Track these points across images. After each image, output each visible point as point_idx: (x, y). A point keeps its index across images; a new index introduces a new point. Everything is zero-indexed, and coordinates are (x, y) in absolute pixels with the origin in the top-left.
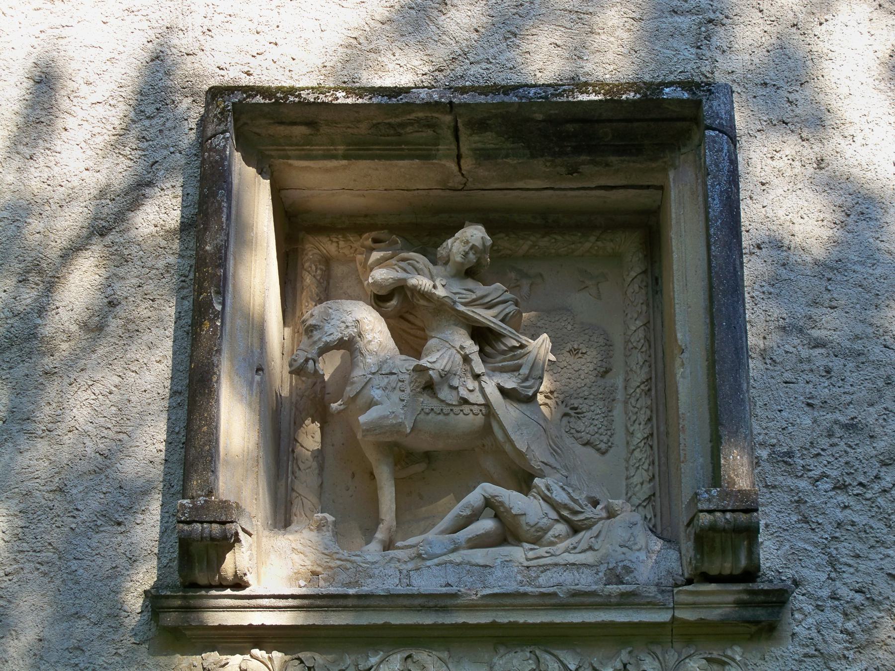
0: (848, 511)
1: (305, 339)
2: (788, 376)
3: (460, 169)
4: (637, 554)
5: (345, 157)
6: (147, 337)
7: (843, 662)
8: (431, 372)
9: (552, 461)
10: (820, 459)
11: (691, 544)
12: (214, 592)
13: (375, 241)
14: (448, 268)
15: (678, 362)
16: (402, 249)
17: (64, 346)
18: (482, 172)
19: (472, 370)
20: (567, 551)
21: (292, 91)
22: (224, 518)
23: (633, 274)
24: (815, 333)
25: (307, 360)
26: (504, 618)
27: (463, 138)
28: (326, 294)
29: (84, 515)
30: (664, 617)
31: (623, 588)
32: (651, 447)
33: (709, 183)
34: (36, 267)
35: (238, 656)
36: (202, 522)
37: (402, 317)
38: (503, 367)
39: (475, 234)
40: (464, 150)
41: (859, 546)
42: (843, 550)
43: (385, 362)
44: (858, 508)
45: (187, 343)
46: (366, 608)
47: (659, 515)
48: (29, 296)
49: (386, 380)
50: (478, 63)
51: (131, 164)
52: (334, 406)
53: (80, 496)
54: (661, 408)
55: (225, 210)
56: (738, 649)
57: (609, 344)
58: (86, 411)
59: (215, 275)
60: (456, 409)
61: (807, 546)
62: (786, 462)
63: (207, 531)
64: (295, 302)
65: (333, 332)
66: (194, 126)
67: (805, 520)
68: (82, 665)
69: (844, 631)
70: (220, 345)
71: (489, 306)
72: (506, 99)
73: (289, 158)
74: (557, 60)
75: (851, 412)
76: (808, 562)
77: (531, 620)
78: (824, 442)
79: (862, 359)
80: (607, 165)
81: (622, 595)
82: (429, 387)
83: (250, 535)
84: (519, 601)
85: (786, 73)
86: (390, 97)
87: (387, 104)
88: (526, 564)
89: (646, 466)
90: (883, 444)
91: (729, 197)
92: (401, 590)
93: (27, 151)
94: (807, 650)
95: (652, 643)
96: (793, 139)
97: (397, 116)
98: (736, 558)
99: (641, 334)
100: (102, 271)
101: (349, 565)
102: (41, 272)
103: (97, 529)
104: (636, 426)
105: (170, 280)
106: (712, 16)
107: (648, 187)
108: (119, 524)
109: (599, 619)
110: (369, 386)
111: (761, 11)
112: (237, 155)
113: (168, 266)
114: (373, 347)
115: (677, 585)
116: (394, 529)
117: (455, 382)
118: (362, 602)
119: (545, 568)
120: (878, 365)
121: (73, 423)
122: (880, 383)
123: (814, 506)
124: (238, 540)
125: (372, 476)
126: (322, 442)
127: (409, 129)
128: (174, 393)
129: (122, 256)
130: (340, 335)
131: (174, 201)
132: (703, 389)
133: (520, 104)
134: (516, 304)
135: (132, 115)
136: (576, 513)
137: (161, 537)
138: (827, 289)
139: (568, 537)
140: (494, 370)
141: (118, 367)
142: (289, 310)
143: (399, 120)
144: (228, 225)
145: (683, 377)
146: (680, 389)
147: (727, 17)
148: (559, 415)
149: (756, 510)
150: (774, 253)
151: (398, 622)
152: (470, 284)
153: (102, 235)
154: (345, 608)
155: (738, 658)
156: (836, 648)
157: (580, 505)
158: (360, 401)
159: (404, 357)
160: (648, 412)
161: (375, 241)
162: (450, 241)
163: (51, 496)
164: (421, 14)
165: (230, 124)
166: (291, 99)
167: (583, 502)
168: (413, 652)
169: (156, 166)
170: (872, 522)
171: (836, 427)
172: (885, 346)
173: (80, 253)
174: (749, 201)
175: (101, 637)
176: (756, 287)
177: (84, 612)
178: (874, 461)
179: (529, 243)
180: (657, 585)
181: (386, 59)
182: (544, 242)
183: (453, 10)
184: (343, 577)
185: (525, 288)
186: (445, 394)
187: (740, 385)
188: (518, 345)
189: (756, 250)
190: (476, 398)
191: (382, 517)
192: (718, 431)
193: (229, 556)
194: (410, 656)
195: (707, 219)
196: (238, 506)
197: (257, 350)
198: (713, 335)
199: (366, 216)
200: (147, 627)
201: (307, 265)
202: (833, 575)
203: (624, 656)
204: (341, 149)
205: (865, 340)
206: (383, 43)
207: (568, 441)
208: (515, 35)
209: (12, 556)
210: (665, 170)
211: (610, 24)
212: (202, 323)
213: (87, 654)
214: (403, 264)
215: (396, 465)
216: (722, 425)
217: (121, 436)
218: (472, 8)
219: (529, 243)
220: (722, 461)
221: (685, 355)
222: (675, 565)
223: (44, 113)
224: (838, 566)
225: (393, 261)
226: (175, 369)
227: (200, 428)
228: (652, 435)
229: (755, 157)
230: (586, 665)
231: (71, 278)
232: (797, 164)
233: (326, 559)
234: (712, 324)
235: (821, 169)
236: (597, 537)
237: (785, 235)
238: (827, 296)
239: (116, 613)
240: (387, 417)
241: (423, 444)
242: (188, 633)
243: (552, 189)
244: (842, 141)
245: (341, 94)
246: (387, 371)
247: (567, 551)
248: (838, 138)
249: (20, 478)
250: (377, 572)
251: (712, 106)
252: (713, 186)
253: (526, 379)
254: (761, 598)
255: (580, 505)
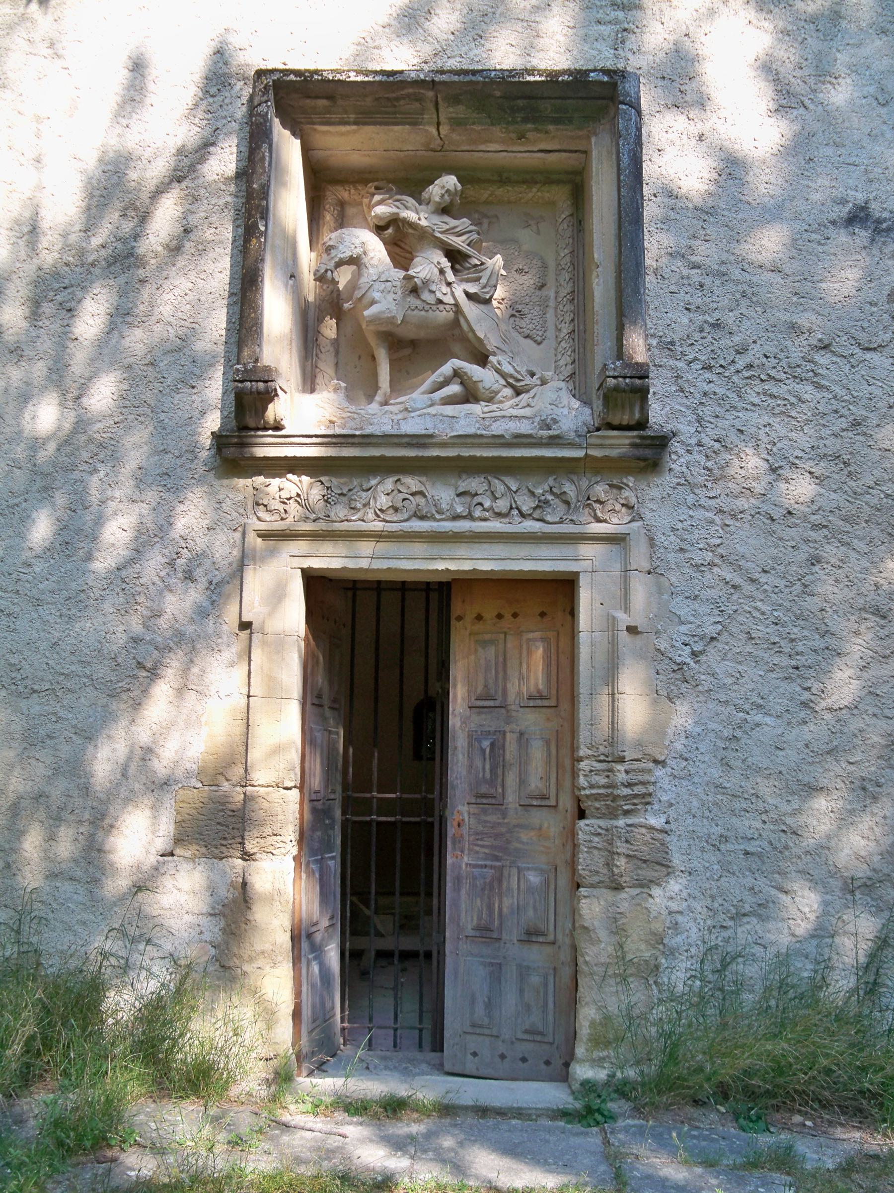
0: (711, 385)
1: (325, 256)
2: (673, 288)
3: (439, 134)
4: (562, 410)
5: (355, 123)
6: (212, 255)
7: (704, 489)
8: (416, 280)
9: (502, 346)
10: (694, 347)
11: (600, 402)
12: (260, 433)
13: (377, 188)
14: (429, 206)
15: (595, 274)
16: (396, 194)
17: (153, 261)
18: (455, 136)
19: (446, 279)
20: (512, 407)
21: (316, 72)
22: (266, 378)
23: (563, 216)
24: (694, 259)
25: (326, 271)
26: (466, 453)
27: (441, 110)
28: (342, 223)
29: (169, 381)
30: (580, 453)
31: (551, 432)
32: (573, 339)
33: (621, 143)
34: (132, 206)
35: (277, 479)
36: (251, 381)
37: (396, 244)
38: (468, 278)
39: (450, 181)
40: (442, 119)
41: (718, 409)
42: (707, 412)
43: (383, 273)
44: (719, 382)
45: (240, 259)
46: (368, 445)
47: (577, 388)
48: (128, 227)
49: (383, 286)
50: (454, 57)
51: (199, 130)
52: (346, 306)
53: (165, 368)
54: (581, 313)
55: (267, 158)
56: (631, 479)
57: (545, 266)
58: (168, 308)
59: (260, 205)
60: (434, 307)
61: (682, 408)
62: (669, 349)
63: (255, 387)
64: (318, 230)
65: (345, 252)
66: (245, 102)
67: (682, 390)
68: (169, 486)
69: (706, 468)
70: (264, 255)
71: (459, 235)
72: (474, 78)
73: (314, 124)
74: (512, 56)
75: (717, 315)
76: (682, 420)
77: (485, 455)
78: (697, 336)
79: (726, 278)
80: (547, 132)
81: (551, 437)
82: (415, 291)
83: (286, 392)
84: (477, 441)
85: (679, 71)
86: (388, 76)
87: (386, 82)
88: (482, 416)
89: (569, 353)
90: (738, 338)
91: (635, 154)
92: (394, 432)
93: (124, 122)
94: (679, 480)
95: (570, 473)
96: (682, 119)
97: (393, 92)
98: (632, 413)
99: (568, 259)
100: (179, 208)
101: (356, 416)
102: (136, 209)
103: (177, 391)
104: (563, 325)
105: (229, 215)
106: (626, 26)
107: (576, 151)
108: (193, 387)
109: (533, 455)
110: (371, 290)
111: (662, 23)
112: (276, 121)
113: (226, 203)
114: (375, 262)
115: (589, 432)
116: (388, 394)
117: (433, 288)
118: (364, 440)
119: (495, 419)
120: (737, 282)
121: (159, 316)
122: (738, 296)
123: (688, 380)
124: (277, 395)
125: (373, 358)
126: (337, 334)
127: (402, 102)
128: (231, 295)
129: (194, 197)
130: (350, 254)
131: (231, 157)
132: (612, 294)
133: (484, 83)
134: (478, 234)
135: (200, 94)
136: (518, 380)
137: (223, 396)
138: (702, 228)
139: (512, 398)
140: (462, 281)
141: (192, 276)
142: (314, 240)
143: (394, 95)
144: (270, 170)
145: (598, 284)
146: (596, 293)
147: (637, 27)
148: (508, 317)
149: (647, 377)
150: (666, 200)
151: (390, 455)
152: (447, 219)
153: (179, 182)
154: (353, 445)
155: (631, 485)
156: (700, 479)
157: (522, 375)
158: (365, 301)
159: (397, 270)
160: (572, 315)
161: (377, 188)
162: (431, 187)
163: (145, 368)
164: (412, 21)
165: (272, 96)
166: (316, 77)
167: (524, 373)
168: (401, 477)
169: (218, 131)
170: (728, 393)
171: (706, 325)
172: (743, 270)
173: (163, 195)
174: (649, 162)
175: (181, 466)
176: (652, 224)
177: (170, 448)
178: (731, 350)
179: (489, 192)
180: (576, 431)
181: (385, 53)
182: (500, 192)
183: (436, 18)
184: (352, 424)
185: (485, 226)
186: (426, 296)
187: (639, 289)
188: (479, 263)
189: (653, 198)
190: (448, 299)
191: (380, 385)
192: (622, 320)
193: (270, 406)
194: (399, 480)
195: (619, 169)
196: (276, 370)
197: (290, 262)
198: (620, 253)
199: (370, 172)
200: (214, 459)
201: (327, 207)
202: (699, 429)
203: (551, 481)
204: (352, 116)
205: (728, 265)
206: (383, 42)
207: (515, 334)
208: (481, 37)
209: (119, 410)
210: (588, 138)
211: (551, 30)
212: (250, 240)
213: (172, 478)
214: (397, 203)
215: (390, 350)
216: (625, 316)
217: (194, 325)
218: (450, 16)
219: (489, 192)
220: (625, 342)
221: (600, 269)
222: (589, 419)
223: (136, 93)
224: (703, 423)
225: (390, 201)
226: (232, 278)
227: (249, 314)
228: (574, 331)
229: (655, 131)
230: (524, 488)
231: (157, 212)
232: (684, 137)
233: (340, 411)
234: (620, 245)
235: (702, 141)
236: (533, 397)
237: (674, 188)
238: (703, 232)
239: (193, 451)
240: (384, 312)
241: (409, 333)
242: (242, 463)
243: (506, 151)
244: (717, 121)
245: (352, 74)
246: (385, 279)
247: (512, 407)
248: (714, 118)
249: (123, 356)
250: (376, 421)
251: (629, 86)
252: (624, 145)
253: (484, 287)
254: (649, 442)
255: (522, 375)
